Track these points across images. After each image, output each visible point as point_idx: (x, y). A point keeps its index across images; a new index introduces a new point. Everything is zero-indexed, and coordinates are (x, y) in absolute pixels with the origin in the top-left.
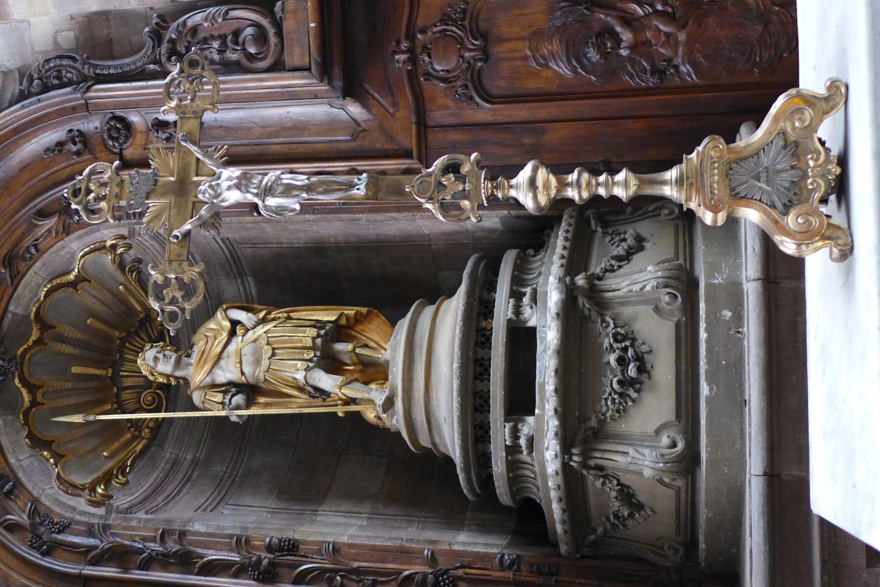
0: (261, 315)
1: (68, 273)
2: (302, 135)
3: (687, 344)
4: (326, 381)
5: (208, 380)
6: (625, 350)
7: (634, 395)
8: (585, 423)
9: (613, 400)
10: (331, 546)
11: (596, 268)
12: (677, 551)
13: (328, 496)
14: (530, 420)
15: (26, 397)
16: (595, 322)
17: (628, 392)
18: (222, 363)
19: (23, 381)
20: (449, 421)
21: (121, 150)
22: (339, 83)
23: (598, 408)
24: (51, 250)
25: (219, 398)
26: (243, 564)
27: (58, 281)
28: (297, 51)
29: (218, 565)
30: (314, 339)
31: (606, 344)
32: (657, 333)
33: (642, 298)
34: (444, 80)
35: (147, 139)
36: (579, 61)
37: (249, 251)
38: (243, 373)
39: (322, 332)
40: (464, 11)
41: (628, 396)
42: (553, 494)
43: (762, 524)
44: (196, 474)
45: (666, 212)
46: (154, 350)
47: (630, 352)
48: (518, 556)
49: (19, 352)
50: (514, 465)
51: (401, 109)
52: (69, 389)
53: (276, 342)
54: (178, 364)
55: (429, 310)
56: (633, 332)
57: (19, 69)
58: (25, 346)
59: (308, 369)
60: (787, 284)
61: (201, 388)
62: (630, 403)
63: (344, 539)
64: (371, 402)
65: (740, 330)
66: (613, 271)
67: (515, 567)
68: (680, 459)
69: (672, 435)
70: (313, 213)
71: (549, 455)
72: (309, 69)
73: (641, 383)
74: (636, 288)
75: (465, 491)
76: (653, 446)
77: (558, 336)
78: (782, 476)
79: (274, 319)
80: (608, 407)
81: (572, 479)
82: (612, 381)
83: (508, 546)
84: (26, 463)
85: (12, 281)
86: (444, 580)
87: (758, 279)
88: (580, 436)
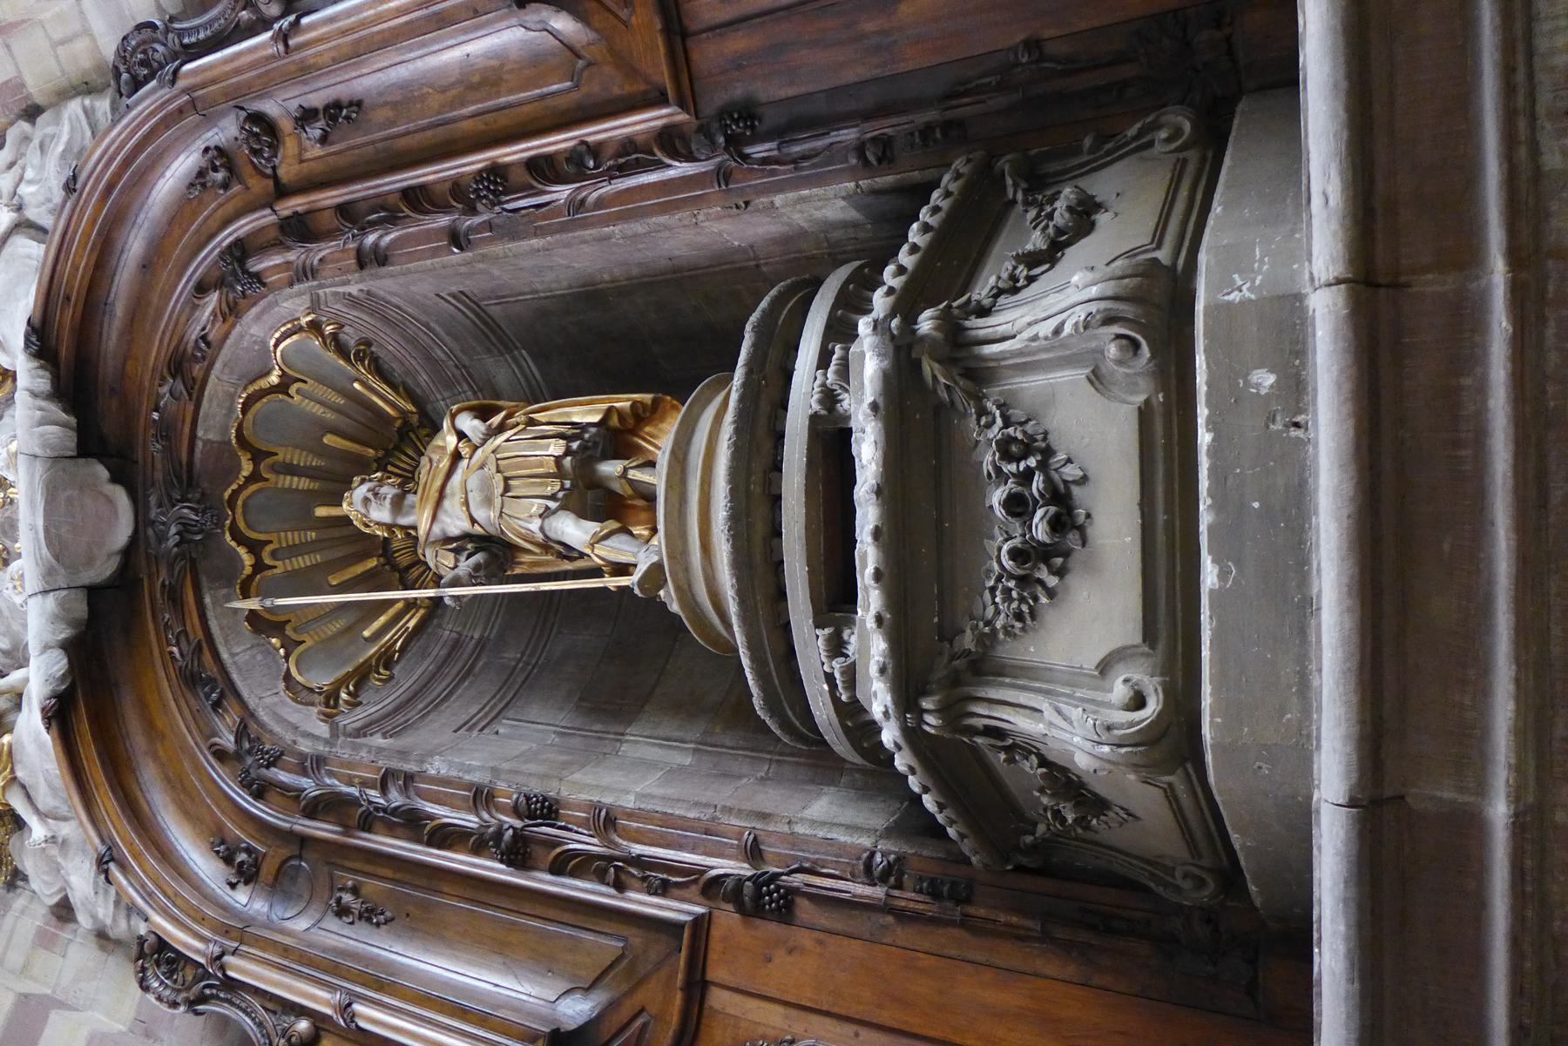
1: (268, 373)
2: (498, 95)
3: (1168, 458)
6: (1026, 477)
7: (1052, 581)
8: (951, 642)
9: (1007, 591)
10: (603, 813)
12: (1200, 883)
13: (647, 708)
15: (247, 560)
16: (965, 415)
17: (1037, 575)
21: (274, 168)
23: (978, 611)
24: (229, 342)
29: (453, 833)
30: (558, 460)
31: (987, 467)
32: (1096, 434)
33: (1056, 351)
35: (300, 144)
38: (473, 521)
39: (575, 445)
41: (1041, 582)
43: (1342, 928)
44: (481, 663)
45: (1163, 134)
47: (1038, 482)
48: (900, 859)
49: (227, 495)
51: (639, 10)
52: (313, 542)
53: (509, 467)
54: (398, 504)
56: (1046, 433)
58: (234, 486)
59: (546, 514)
60: (1431, 285)
62: (1044, 600)
63: (629, 802)
65: (1299, 419)
66: (1015, 290)
67: (892, 879)
68: (1150, 738)
69: (1136, 677)
70: (536, 235)
73: (1067, 554)
74: (1046, 329)
76: (1093, 701)
77: (879, 454)
78: (1409, 799)
80: (996, 609)
82: (1000, 549)
83: (889, 833)
84: (241, 659)
85: (190, 395)
86: (770, 893)
87: (1338, 282)
88: (940, 673)
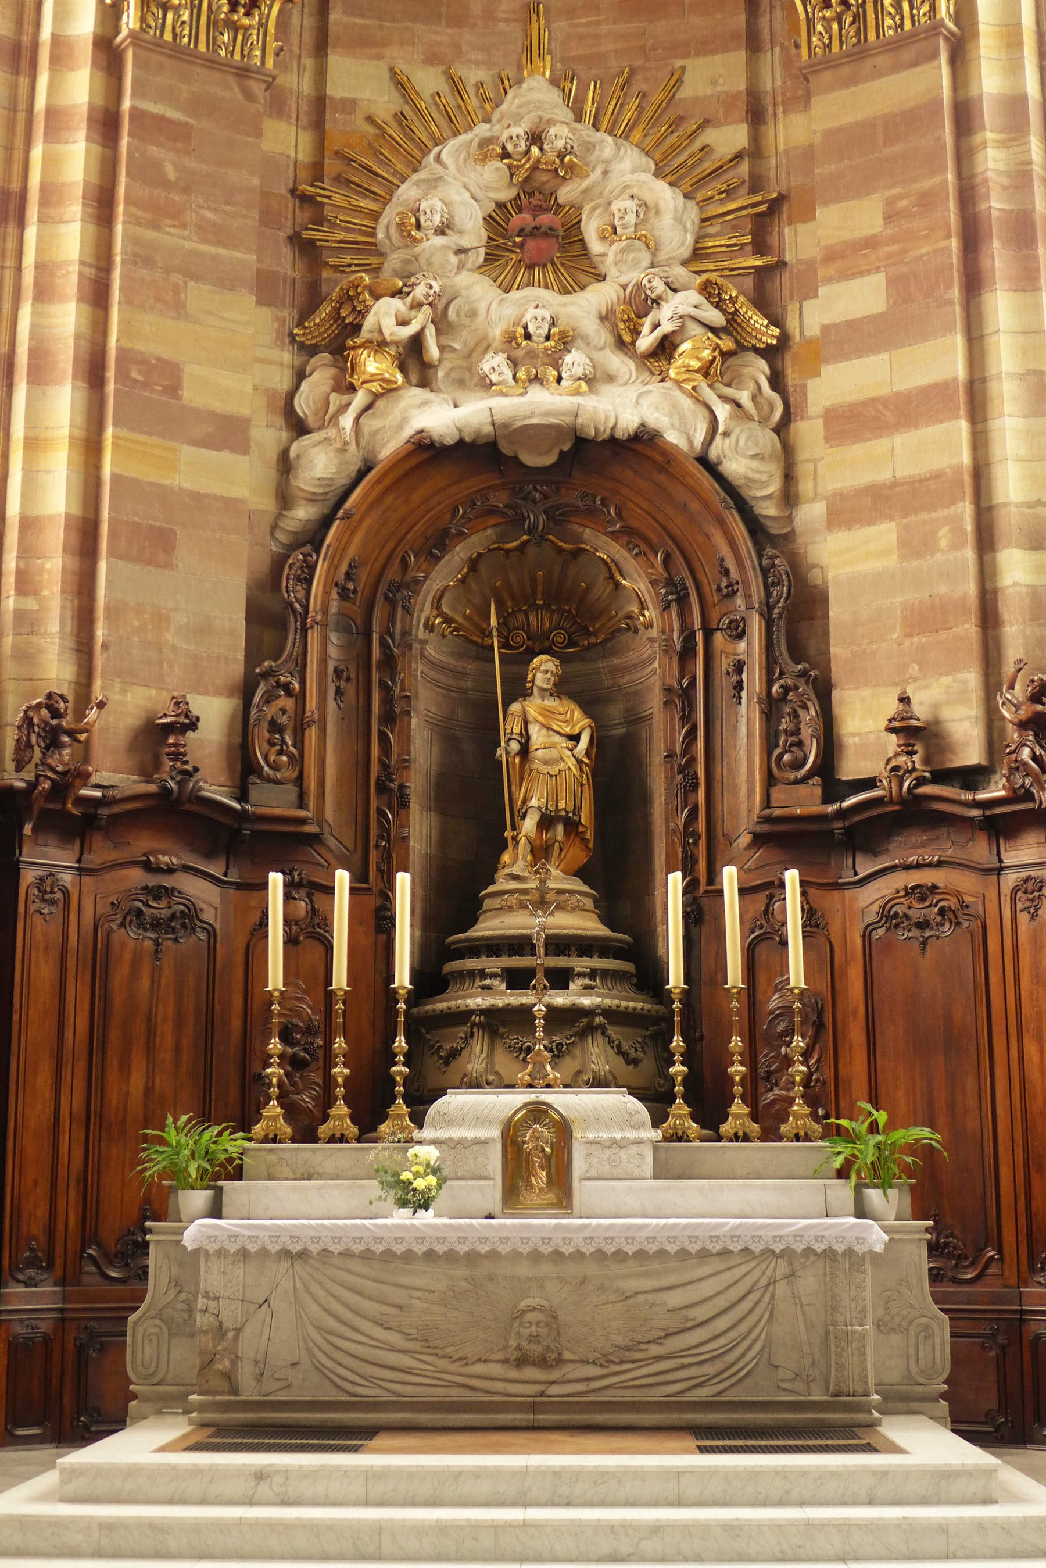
0: (585, 760)
4: (529, 825)
5: (530, 719)
11: (611, 1030)
12: (417, 1091)
14: (503, 986)
18: (544, 731)
19: (525, 544)
20: (502, 925)
22: (758, 829)
25: (516, 730)
26: (389, 766)
27: (614, 567)
28: (782, 796)
34: (766, 911)
36: (777, 1016)
37: (644, 735)
40: (817, 926)
42: (453, 1003)
46: (554, 669)
49: (550, 537)
50: (472, 975)
55: (589, 903)
57: (793, 532)
61: (524, 712)
63: (412, 844)
64: (515, 862)
71: (479, 1000)
72: (768, 807)
75: (452, 938)
79: (581, 770)
81: (462, 1017)
